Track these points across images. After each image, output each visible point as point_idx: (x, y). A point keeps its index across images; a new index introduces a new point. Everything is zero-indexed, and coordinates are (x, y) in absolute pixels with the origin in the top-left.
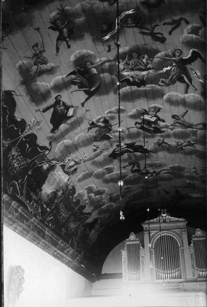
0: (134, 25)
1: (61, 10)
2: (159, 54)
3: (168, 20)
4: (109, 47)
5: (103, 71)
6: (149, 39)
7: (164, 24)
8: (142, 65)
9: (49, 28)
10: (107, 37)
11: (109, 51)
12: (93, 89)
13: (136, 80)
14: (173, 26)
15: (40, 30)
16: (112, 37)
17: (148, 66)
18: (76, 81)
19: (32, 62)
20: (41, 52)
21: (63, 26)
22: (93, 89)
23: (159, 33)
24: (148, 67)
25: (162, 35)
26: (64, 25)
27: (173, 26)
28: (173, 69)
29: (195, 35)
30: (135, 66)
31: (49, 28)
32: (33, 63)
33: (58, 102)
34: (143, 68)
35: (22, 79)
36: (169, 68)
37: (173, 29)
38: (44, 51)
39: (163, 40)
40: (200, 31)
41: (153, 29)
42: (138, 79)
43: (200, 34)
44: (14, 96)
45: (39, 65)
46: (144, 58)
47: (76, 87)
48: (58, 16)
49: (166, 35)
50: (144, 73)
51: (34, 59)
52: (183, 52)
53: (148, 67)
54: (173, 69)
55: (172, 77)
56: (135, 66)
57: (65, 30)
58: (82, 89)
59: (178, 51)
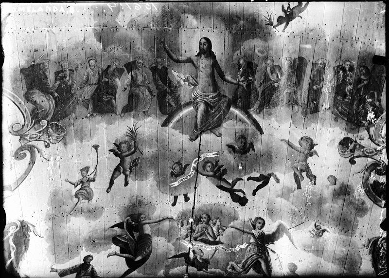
0: (212, 173)
1: (132, 132)
2: (235, 221)
3: (256, 175)
4: (176, 198)
5: (159, 233)
6: (226, 197)
7: (249, 179)
8: (210, 236)
9: (110, 151)
10: (176, 184)
11: (174, 205)
12: (139, 258)
13: (198, 258)
14: (260, 183)
15: (99, 149)
16: (183, 184)
17: (218, 237)
18: (167, 106)
19: (74, 191)
20: (89, 181)
21: (127, 153)
22: (139, 258)
23: (240, 191)
24: (217, 240)
25: (244, 193)
26: (129, 152)
27: (260, 183)
28: (248, 249)
29: (285, 199)
30: (201, 235)
31: (110, 151)
32: (74, 194)
33: (87, 259)
34: (211, 239)
35: (51, 212)
36: (244, 246)
37: (259, 187)
38: (94, 180)
39: (243, 202)
40: (292, 195)
41: (234, 183)
42: (201, 258)
43: (291, 199)
44: (31, 234)
45: (81, 199)
46: (215, 224)
47: (115, 248)
48: (127, 138)
49: (249, 195)
50: (210, 249)
51: (79, 187)
52: (266, 223)
53: (217, 240)
54: (248, 249)
55: (246, 262)
56: (201, 235)
57: (128, 159)
58: (124, 255)
59: (260, 221)
